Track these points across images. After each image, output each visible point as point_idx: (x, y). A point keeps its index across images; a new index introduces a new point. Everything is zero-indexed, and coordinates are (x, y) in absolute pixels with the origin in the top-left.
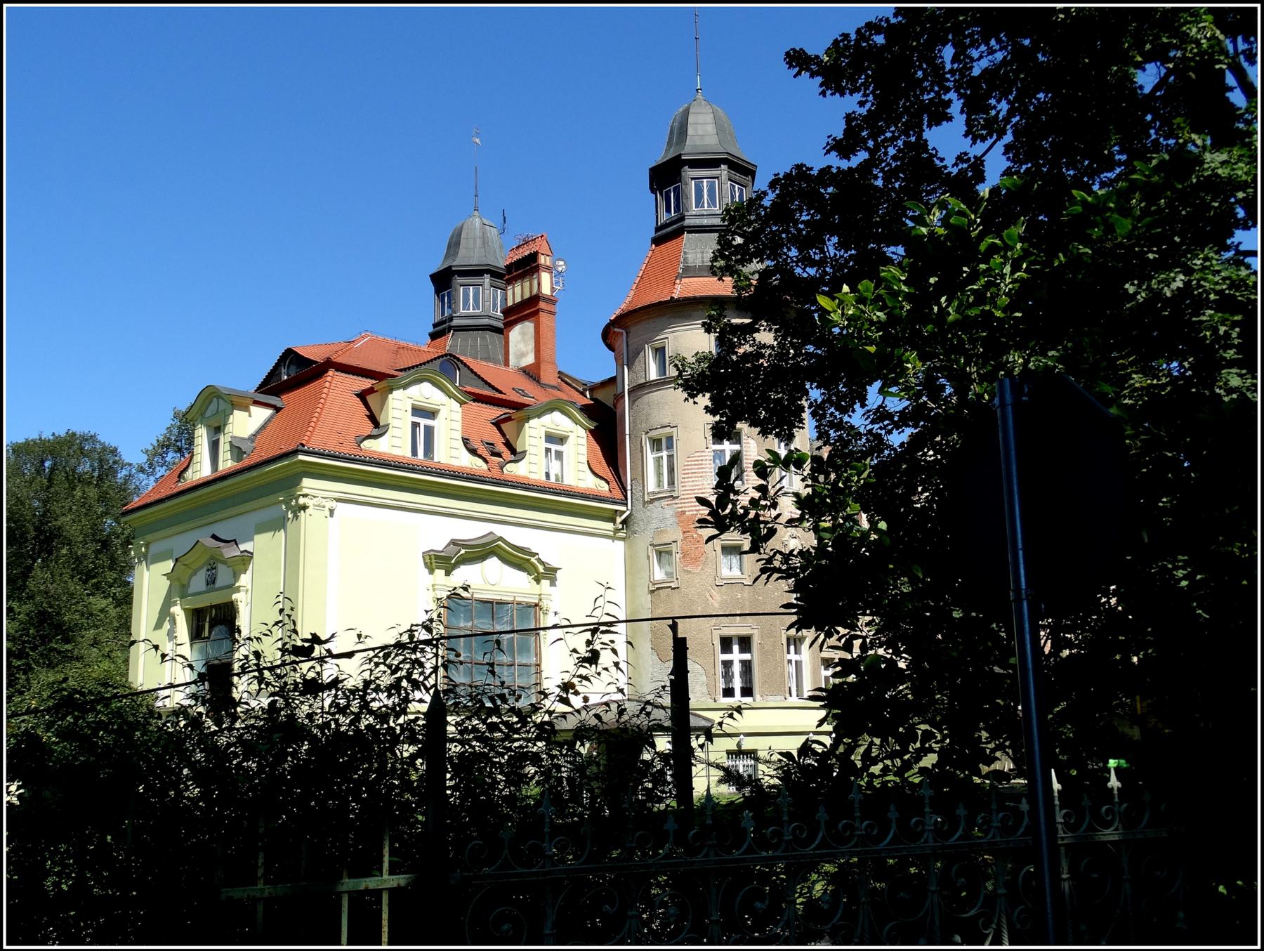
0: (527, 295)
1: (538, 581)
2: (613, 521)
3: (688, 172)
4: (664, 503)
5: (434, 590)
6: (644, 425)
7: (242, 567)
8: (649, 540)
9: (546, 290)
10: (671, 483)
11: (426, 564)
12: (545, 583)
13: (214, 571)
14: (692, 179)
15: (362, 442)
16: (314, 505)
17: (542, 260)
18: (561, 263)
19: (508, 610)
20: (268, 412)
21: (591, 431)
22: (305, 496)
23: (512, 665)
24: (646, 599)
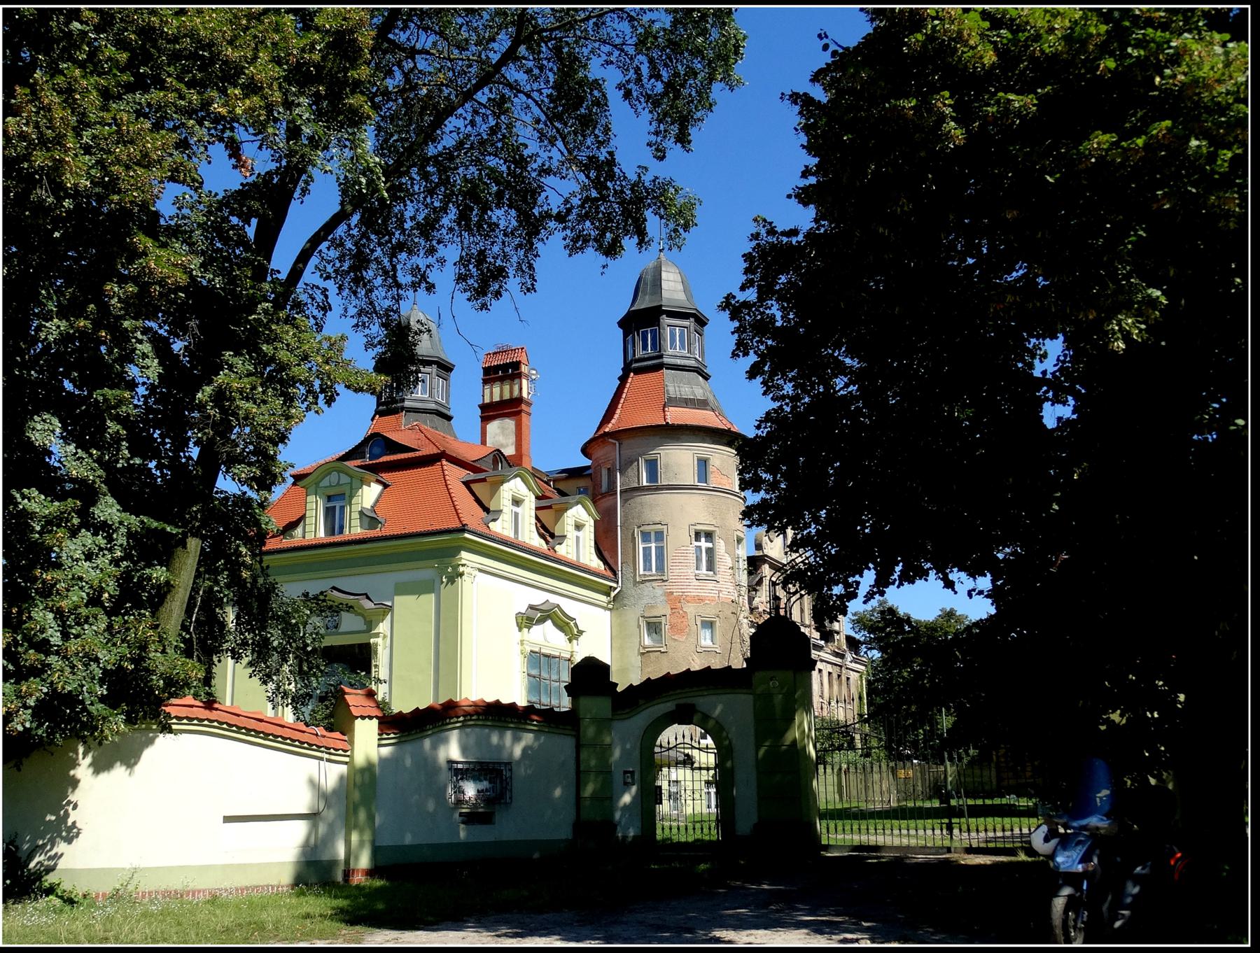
0: (507, 396)
2: (608, 595)
3: (665, 320)
4: (655, 584)
5: (522, 644)
6: (636, 521)
8: (639, 613)
9: (525, 395)
10: (660, 568)
17: (524, 369)
18: (534, 372)
21: (596, 522)
22: (463, 565)
24: (637, 660)
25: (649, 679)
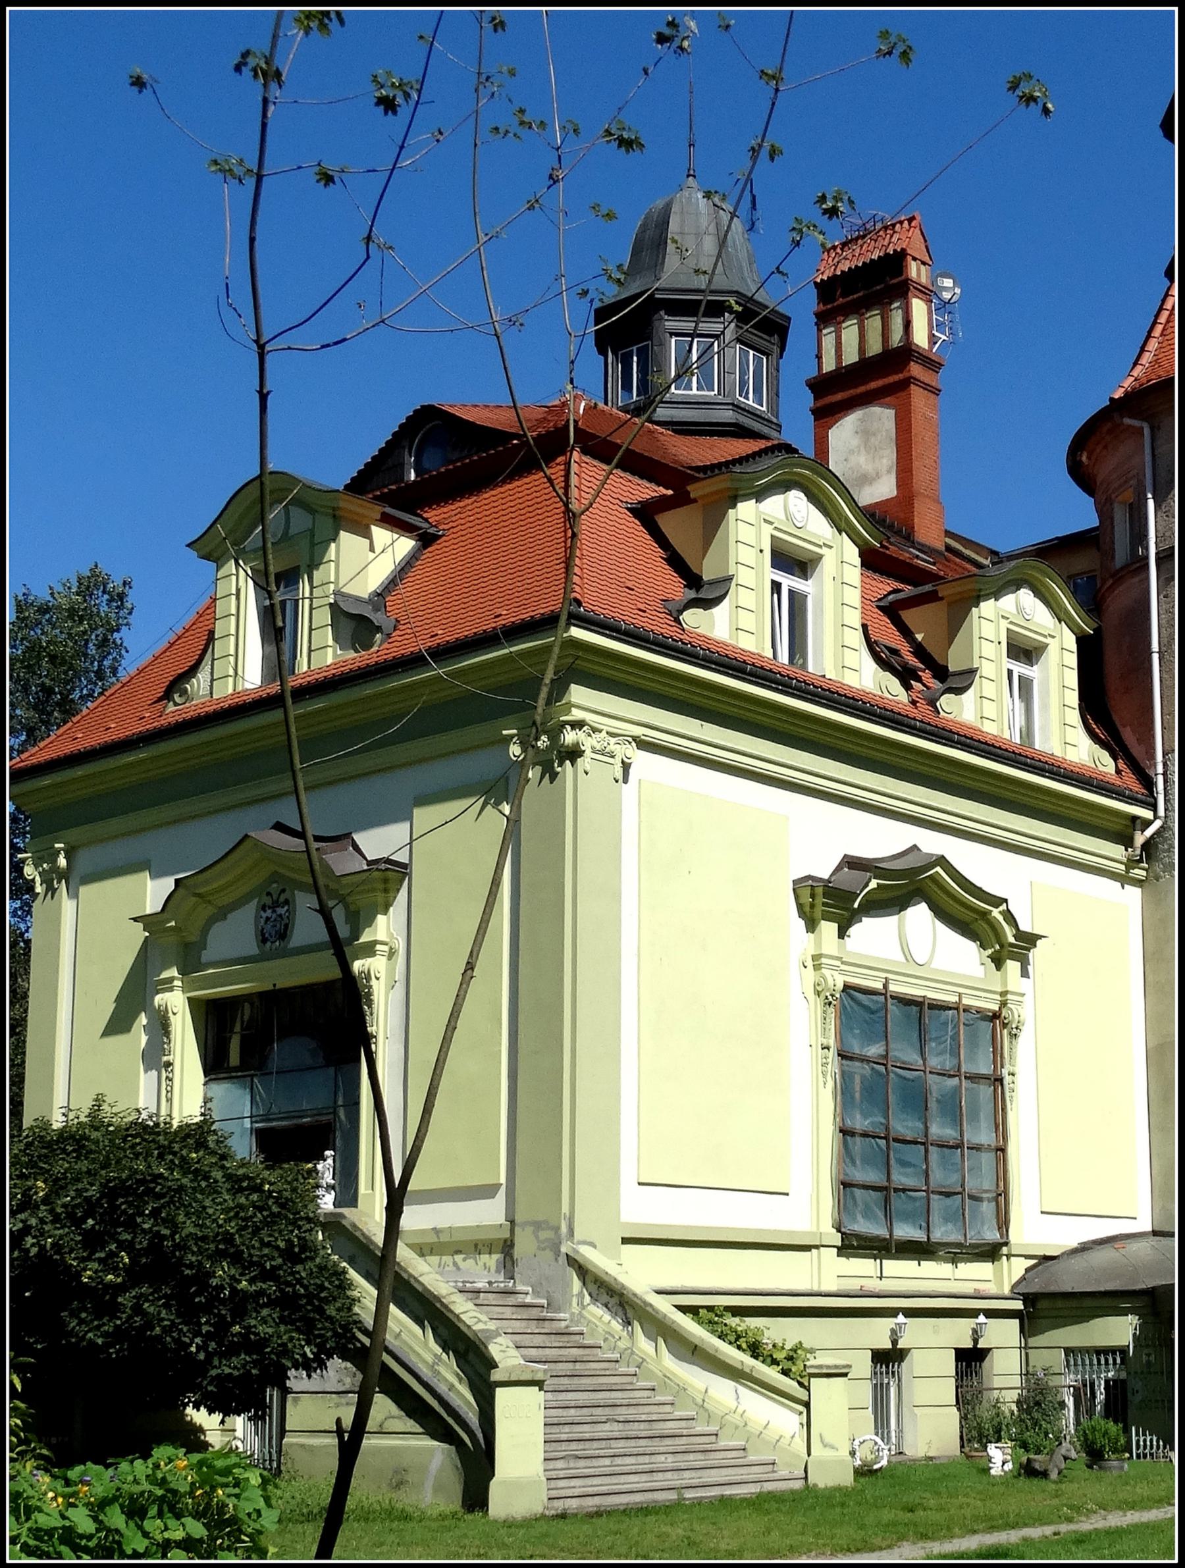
0: (875, 347)
1: (998, 962)
2: (1128, 842)
5: (817, 967)
7: (380, 897)
9: (920, 337)
11: (800, 906)
12: (1012, 966)
13: (282, 911)
14: (671, 334)
15: (681, 612)
16: (594, 751)
17: (914, 270)
18: (948, 283)
19: (946, 1024)
20: (405, 545)
21: (1082, 641)
22: (578, 725)
23: (956, 1147)
25: (370, 926)
